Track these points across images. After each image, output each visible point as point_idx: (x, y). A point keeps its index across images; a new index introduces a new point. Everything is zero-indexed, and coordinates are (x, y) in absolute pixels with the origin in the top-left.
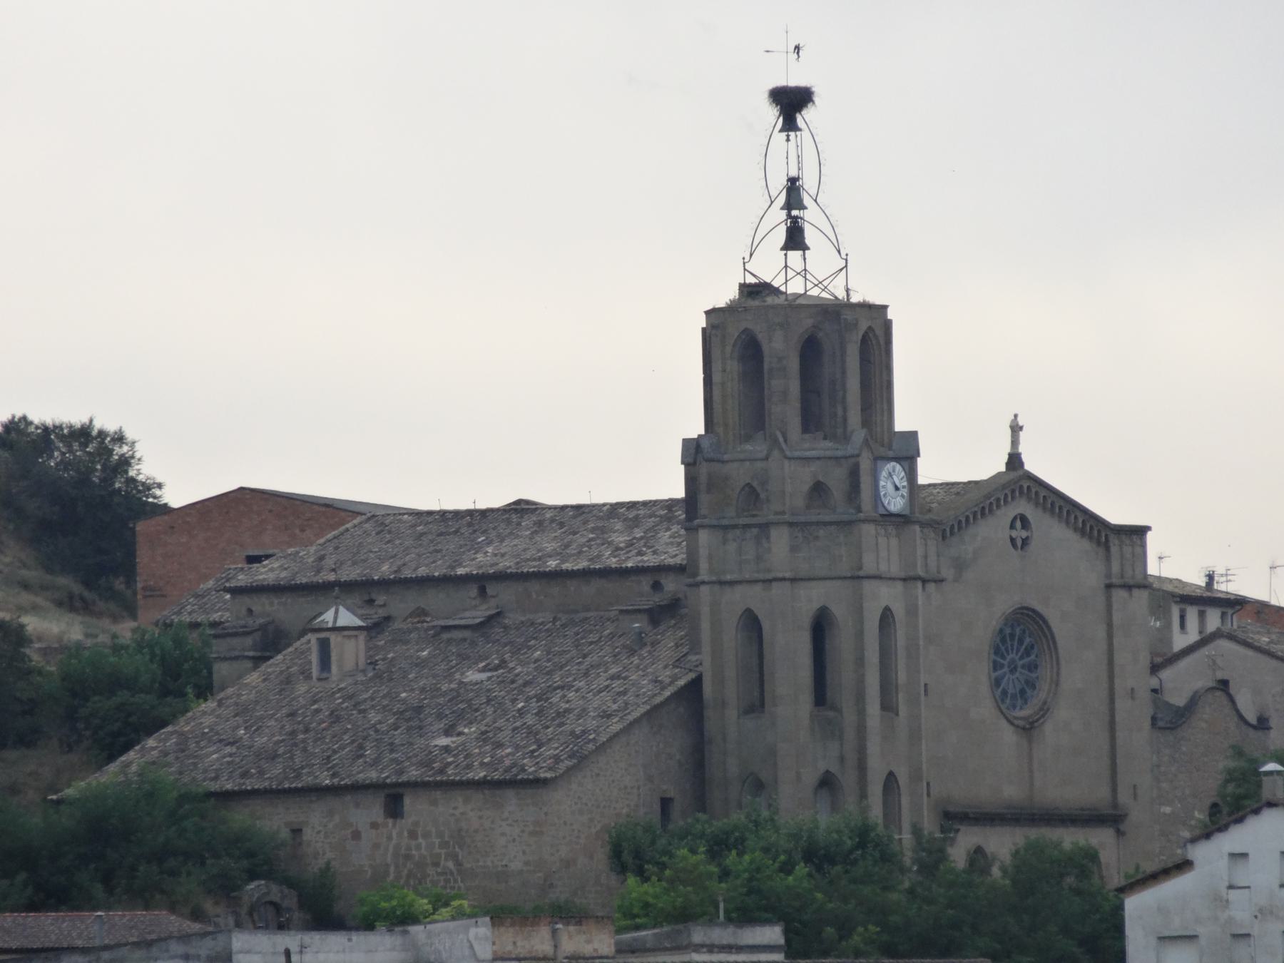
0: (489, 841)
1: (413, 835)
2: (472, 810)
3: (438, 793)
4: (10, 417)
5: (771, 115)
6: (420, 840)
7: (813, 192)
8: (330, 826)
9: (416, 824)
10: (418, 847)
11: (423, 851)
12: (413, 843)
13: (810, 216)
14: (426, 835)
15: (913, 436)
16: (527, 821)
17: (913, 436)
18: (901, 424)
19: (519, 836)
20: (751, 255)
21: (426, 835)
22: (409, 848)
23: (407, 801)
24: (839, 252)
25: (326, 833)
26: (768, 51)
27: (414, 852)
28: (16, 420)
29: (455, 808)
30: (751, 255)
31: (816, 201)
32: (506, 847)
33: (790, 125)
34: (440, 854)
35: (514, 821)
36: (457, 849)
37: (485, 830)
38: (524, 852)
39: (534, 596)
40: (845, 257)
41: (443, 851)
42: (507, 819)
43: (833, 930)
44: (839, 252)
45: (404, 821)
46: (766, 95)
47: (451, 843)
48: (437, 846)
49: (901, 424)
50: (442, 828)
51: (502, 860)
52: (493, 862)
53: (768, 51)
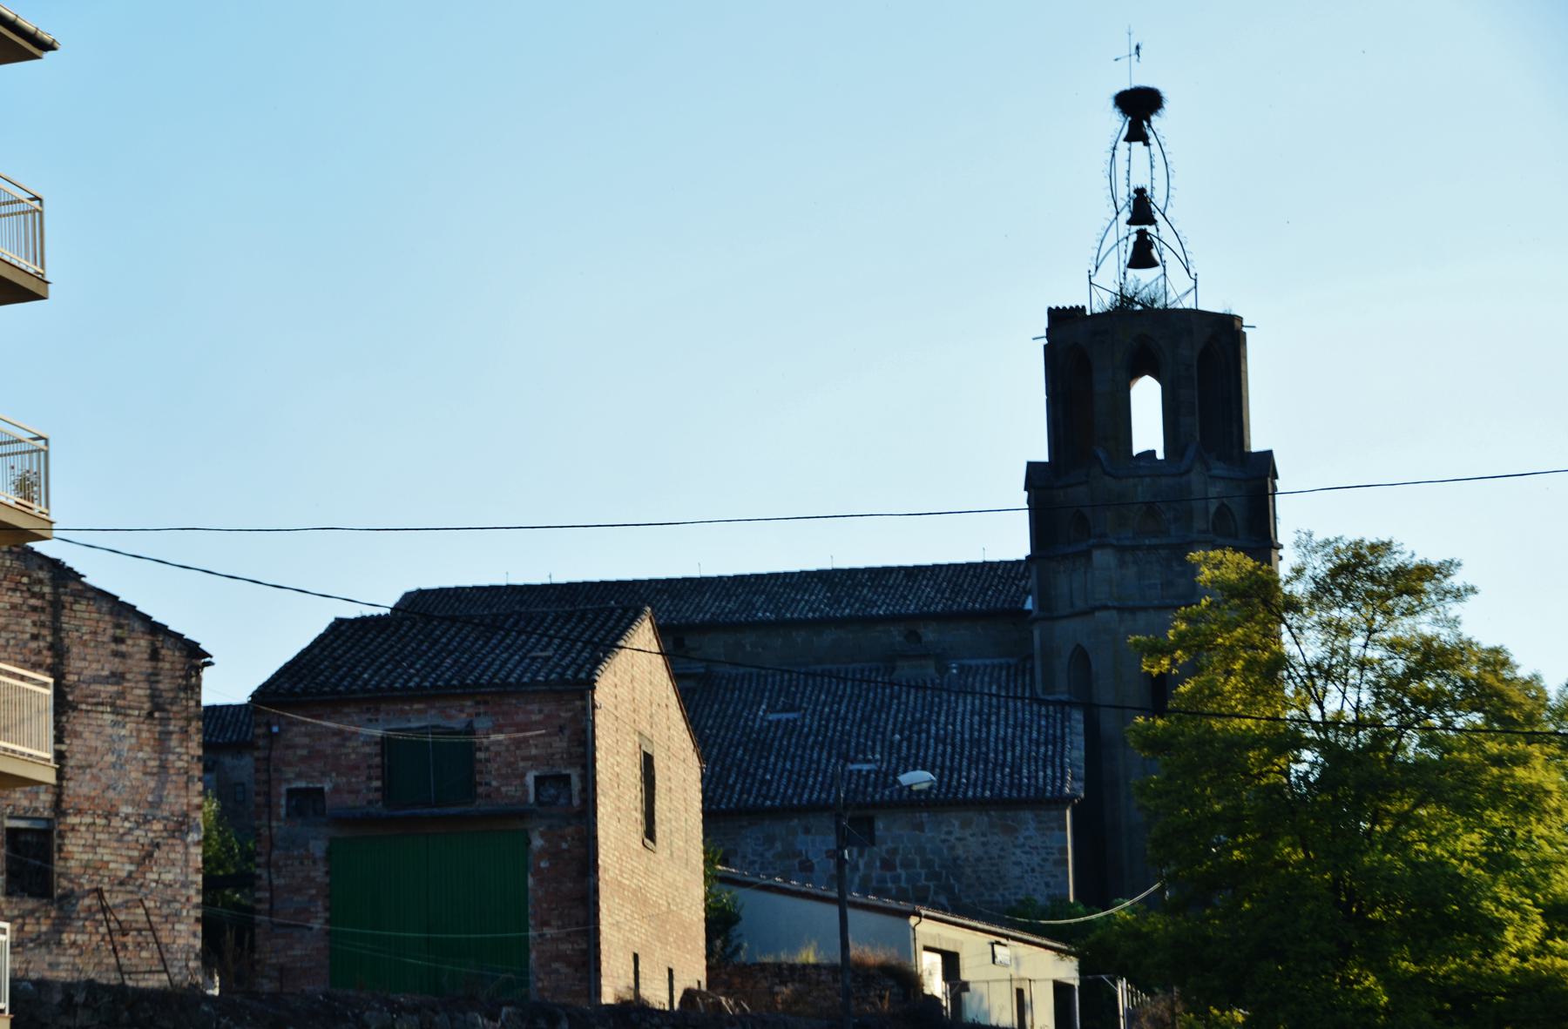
0: (998, 872)
1: (887, 865)
2: (972, 835)
3: (925, 815)
4: (81, 573)
5: (1117, 123)
6: (899, 870)
7: (1161, 205)
8: (769, 855)
9: (894, 851)
10: (896, 879)
11: (903, 884)
12: (888, 875)
13: (1160, 231)
14: (907, 864)
15: (1268, 455)
16: (1051, 848)
17: (1268, 455)
18: (1256, 444)
19: (1039, 865)
20: (1097, 268)
21: (907, 864)
22: (882, 880)
23: (880, 825)
24: (1188, 270)
25: (762, 863)
26: (1116, 60)
27: (890, 885)
28: (83, 579)
29: (949, 833)
30: (1097, 268)
31: (1164, 215)
32: (1022, 878)
33: (1137, 134)
34: (929, 887)
35: (1033, 848)
36: (952, 881)
37: (990, 858)
38: (1047, 885)
39: (748, 648)
40: (1193, 276)
41: (931, 884)
42: (1023, 845)
43: (782, 954)
44: (1188, 270)
45: (875, 849)
46: (1111, 102)
47: (944, 874)
48: (923, 877)
49: (1256, 444)
50: (931, 857)
51: (1016, 894)
52: (1003, 896)
53: (1116, 60)
